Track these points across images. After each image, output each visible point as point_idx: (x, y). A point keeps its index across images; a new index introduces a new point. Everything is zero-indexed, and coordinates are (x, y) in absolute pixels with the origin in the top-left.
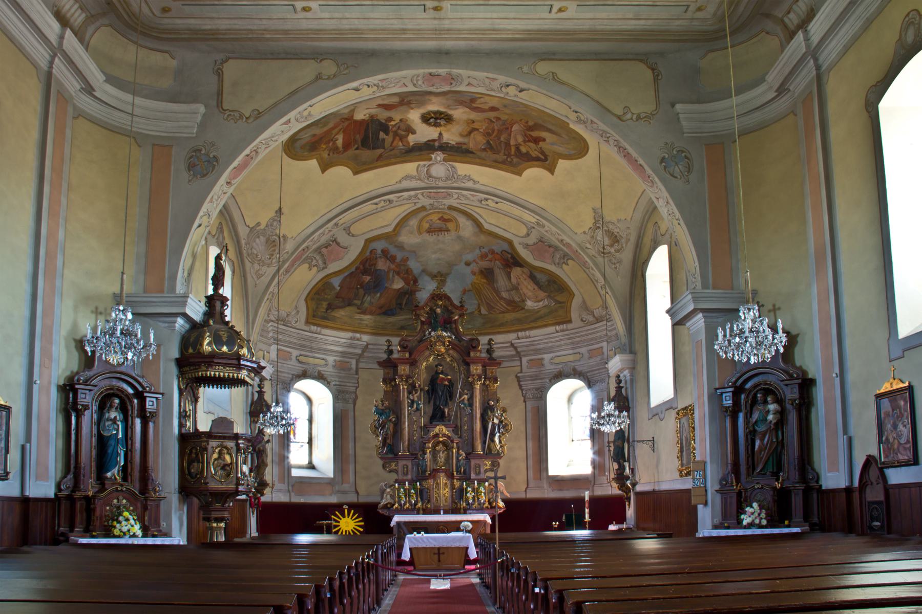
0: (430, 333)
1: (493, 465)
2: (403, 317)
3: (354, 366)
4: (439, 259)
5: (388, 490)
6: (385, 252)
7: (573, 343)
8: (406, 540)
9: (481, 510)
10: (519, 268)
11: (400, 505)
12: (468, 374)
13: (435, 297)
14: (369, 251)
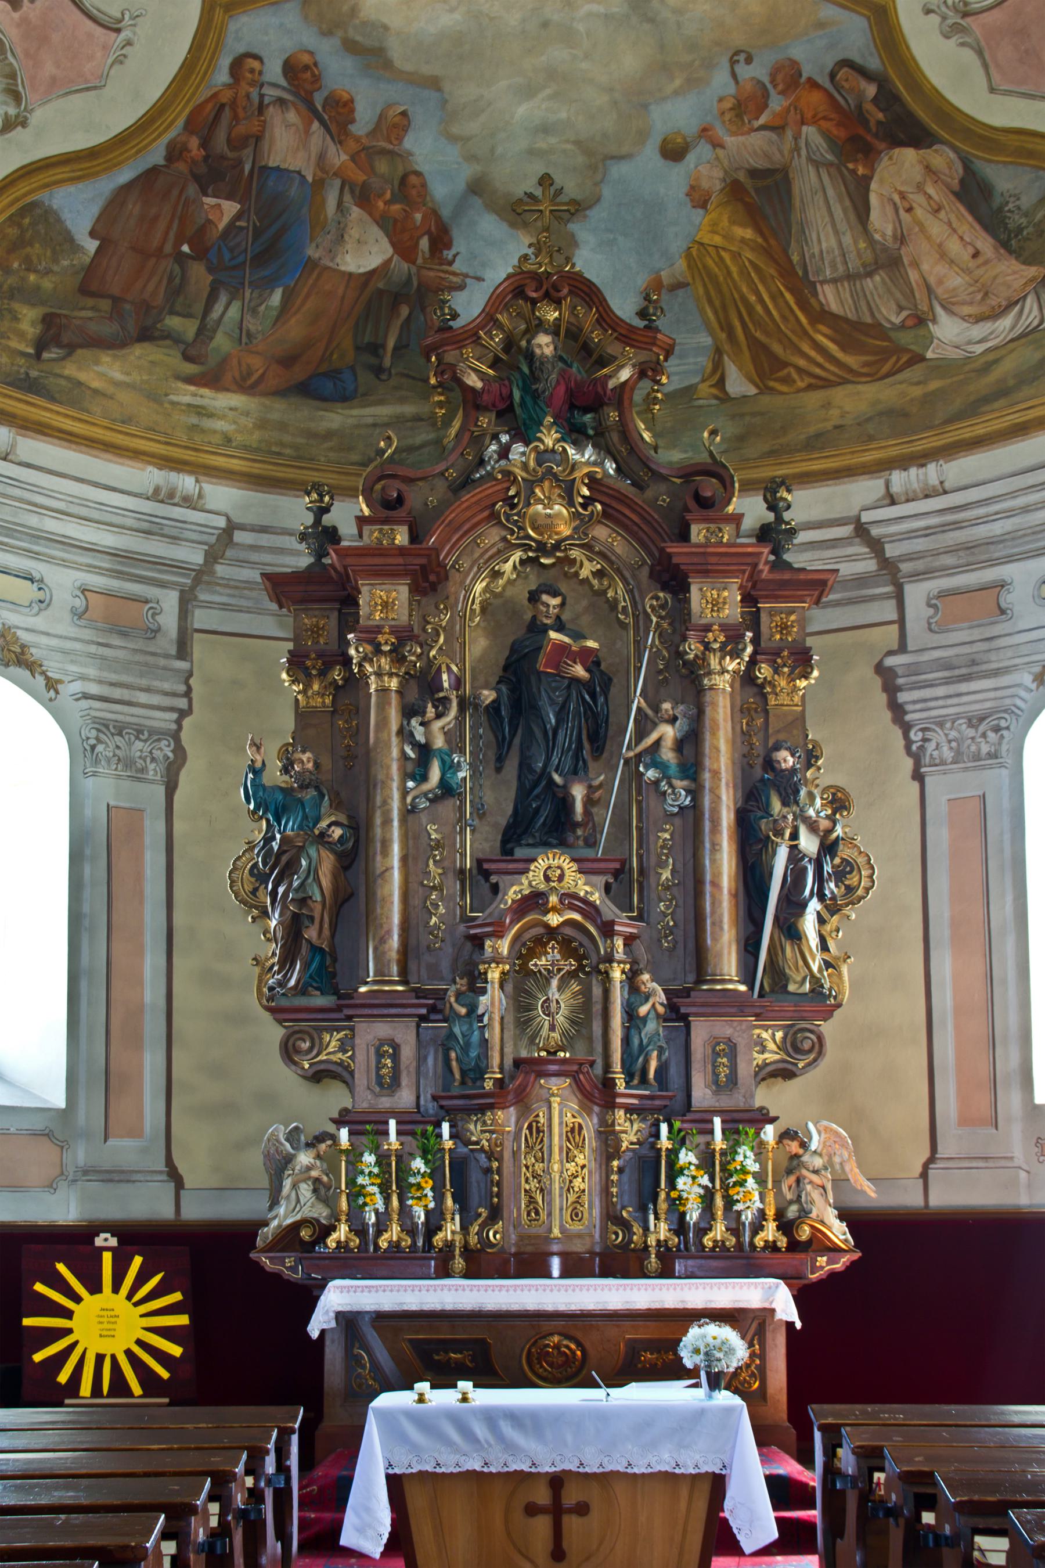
0: (504, 453)
1: (792, 1045)
2: (384, 411)
3: (169, 620)
4: (545, 129)
5: (305, 1158)
6: (300, 73)
8: (372, 1431)
9: (740, 1261)
10: (909, 155)
11: (360, 1230)
12: (680, 618)
13: (524, 289)
14: (225, 62)
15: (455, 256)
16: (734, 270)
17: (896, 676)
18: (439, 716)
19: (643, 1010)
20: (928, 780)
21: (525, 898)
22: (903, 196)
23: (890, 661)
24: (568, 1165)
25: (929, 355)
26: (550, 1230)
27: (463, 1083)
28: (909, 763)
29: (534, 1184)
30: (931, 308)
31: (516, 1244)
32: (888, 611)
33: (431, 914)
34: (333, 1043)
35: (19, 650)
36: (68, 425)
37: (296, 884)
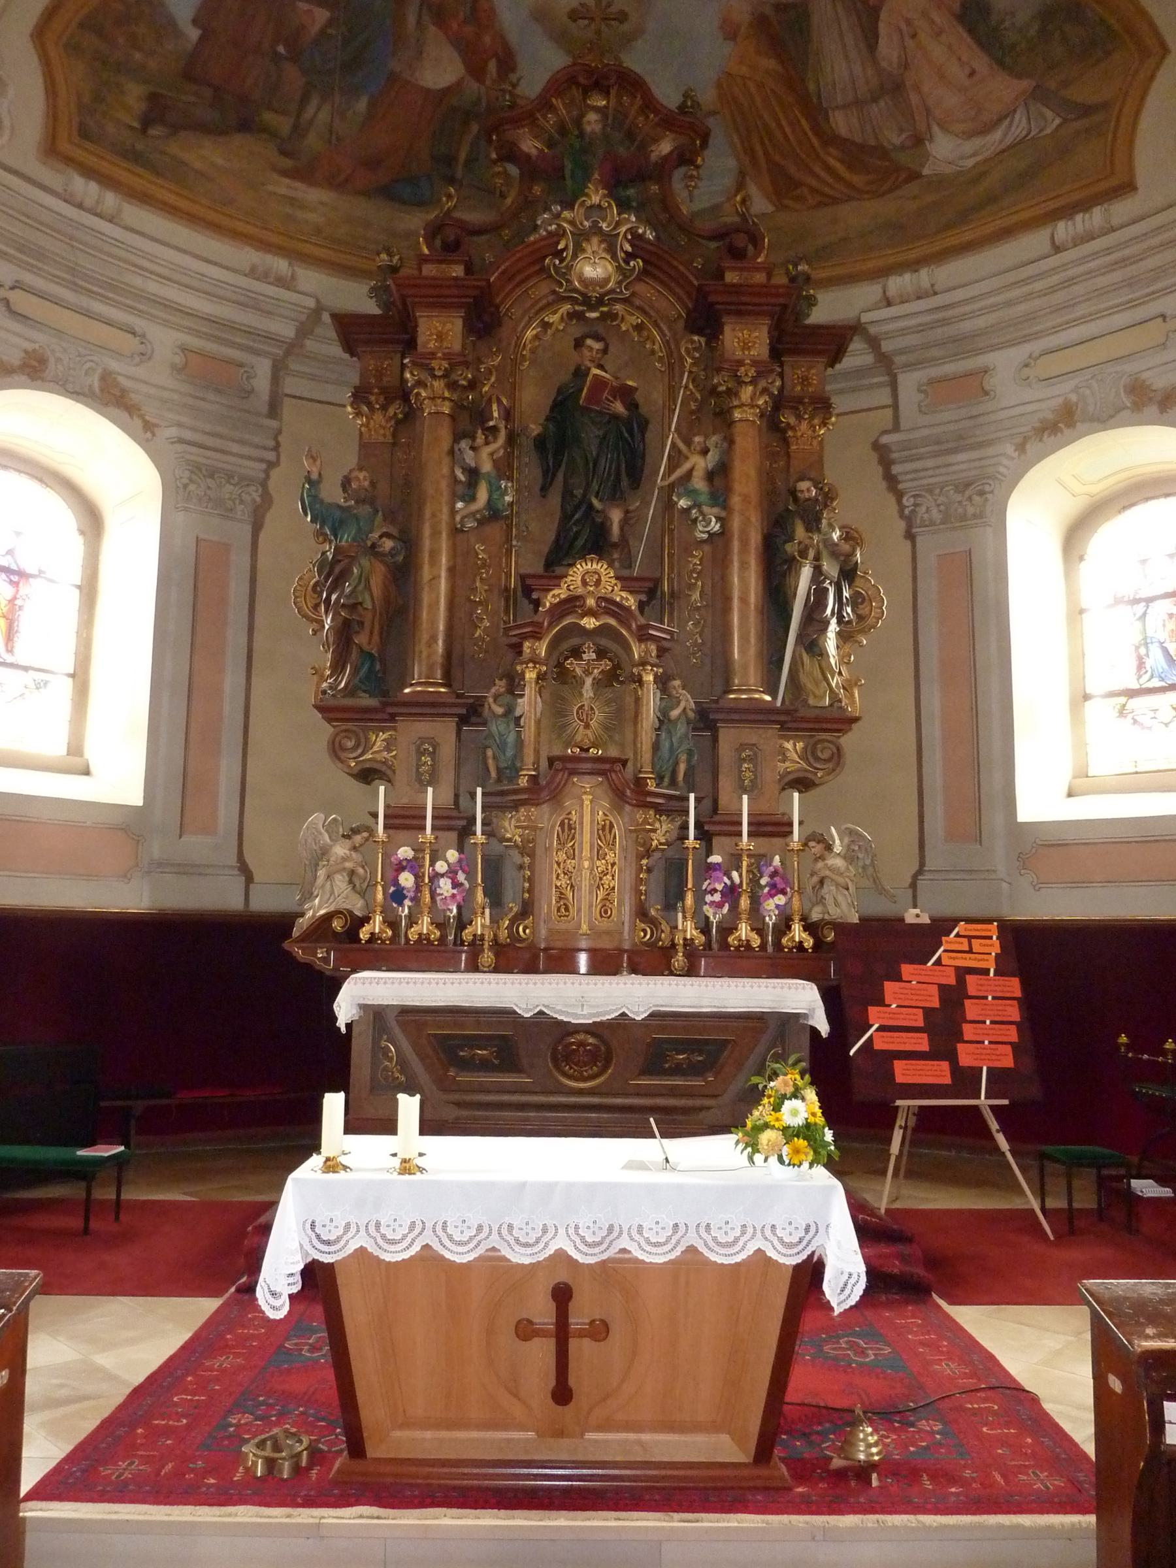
3: (262, 383)
7: (1130, 283)
11: (392, 923)
12: (713, 359)
15: (519, 80)
16: (758, 99)
17: (891, 451)
18: (487, 443)
19: (675, 713)
20: (919, 539)
21: (563, 602)
22: (909, 22)
23: (885, 439)
24: (598, 863)
25: (925, 172)
26: (579, 927)
27: (499, 780)
28: (902, 525)
29: (563, 881)
30: (929, 128)
31: (546, 939)
32: (883, 397)
33: (476, 627)
34: (378, 744)
35: (118, 394)
36: (172, 199)
37: (347, 590)
